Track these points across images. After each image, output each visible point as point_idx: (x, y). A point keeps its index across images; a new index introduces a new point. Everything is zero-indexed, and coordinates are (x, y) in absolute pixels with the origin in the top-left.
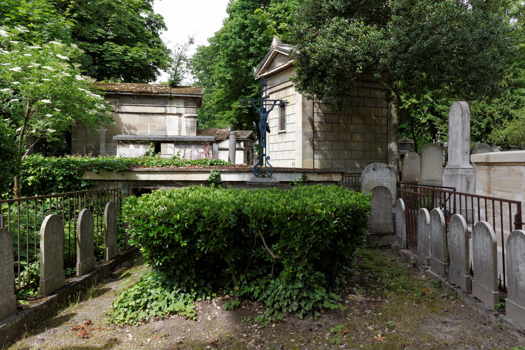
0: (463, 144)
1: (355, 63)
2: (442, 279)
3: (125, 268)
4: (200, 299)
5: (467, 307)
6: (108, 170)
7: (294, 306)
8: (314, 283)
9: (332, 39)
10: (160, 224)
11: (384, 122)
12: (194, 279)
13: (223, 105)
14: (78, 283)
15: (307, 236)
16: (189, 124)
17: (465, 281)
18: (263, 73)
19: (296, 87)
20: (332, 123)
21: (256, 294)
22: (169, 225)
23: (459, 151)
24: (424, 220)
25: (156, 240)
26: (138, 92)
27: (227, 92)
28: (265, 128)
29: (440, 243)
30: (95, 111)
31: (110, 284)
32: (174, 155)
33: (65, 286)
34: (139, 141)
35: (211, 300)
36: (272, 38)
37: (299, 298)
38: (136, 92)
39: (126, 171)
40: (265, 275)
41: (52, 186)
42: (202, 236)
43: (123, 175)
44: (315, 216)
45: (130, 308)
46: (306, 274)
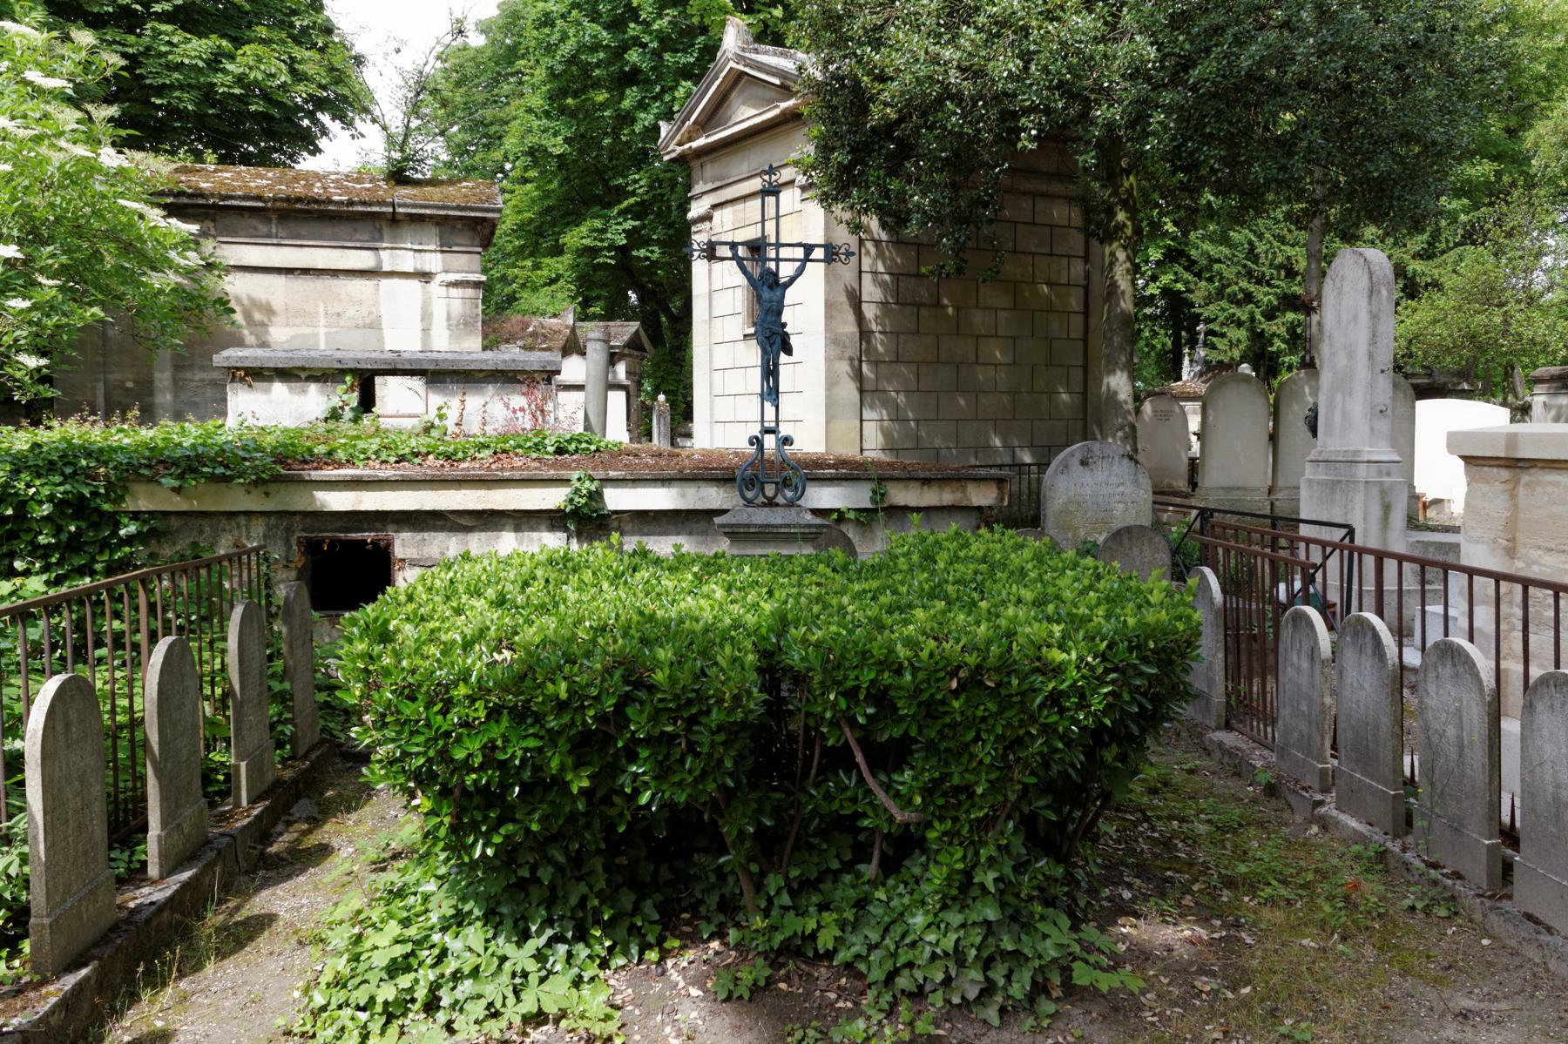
0: (1371, 385)
1: (1015, 116)
2: (1389, 844)
3: (305, 827)
4: (621, 961)
5: (1500, 945)
6: (213, 478)
7: (970, 982)
8: (1031, 898)
9: (940, 35)
10: (494, 714)
11: (1075, 303)
12: (599, 894)
13: (540, 237)
14: (160, 908)
15: (1018, 743)
16: (457, 307)
17: (1484, 858)
18: (690, 140)
19: (803, 189)
20: (919, 305)
21: (825, 940)
22: (521, 715)
23: (1358, 407)
24: (1306, 647)
25: (475, 771)
26: (282, 200)
27: (547, 195)
28: (779, 341)
29: (1377, 727)
30: (173, 278)
31: (265, 893)
32: (426, 418)
33: (115, 928)
34: (303, 369)
35: (661, 961)
36: (723, 24)
37: (985, 954)
38: (275, 200)
39: (278, 479)
40: (848, 867)
41: (12, 536)
42: (644, 753)
43: (267, 494)
44: (1043, 674)
46: (1008, 871)
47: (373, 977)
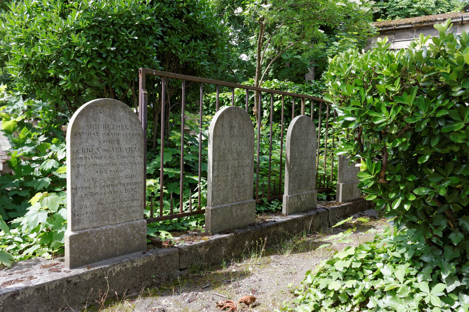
14: (277, 225)
26: (418, 23)
38: (416, 23)
45: (332, 295)
47: (335, 275)
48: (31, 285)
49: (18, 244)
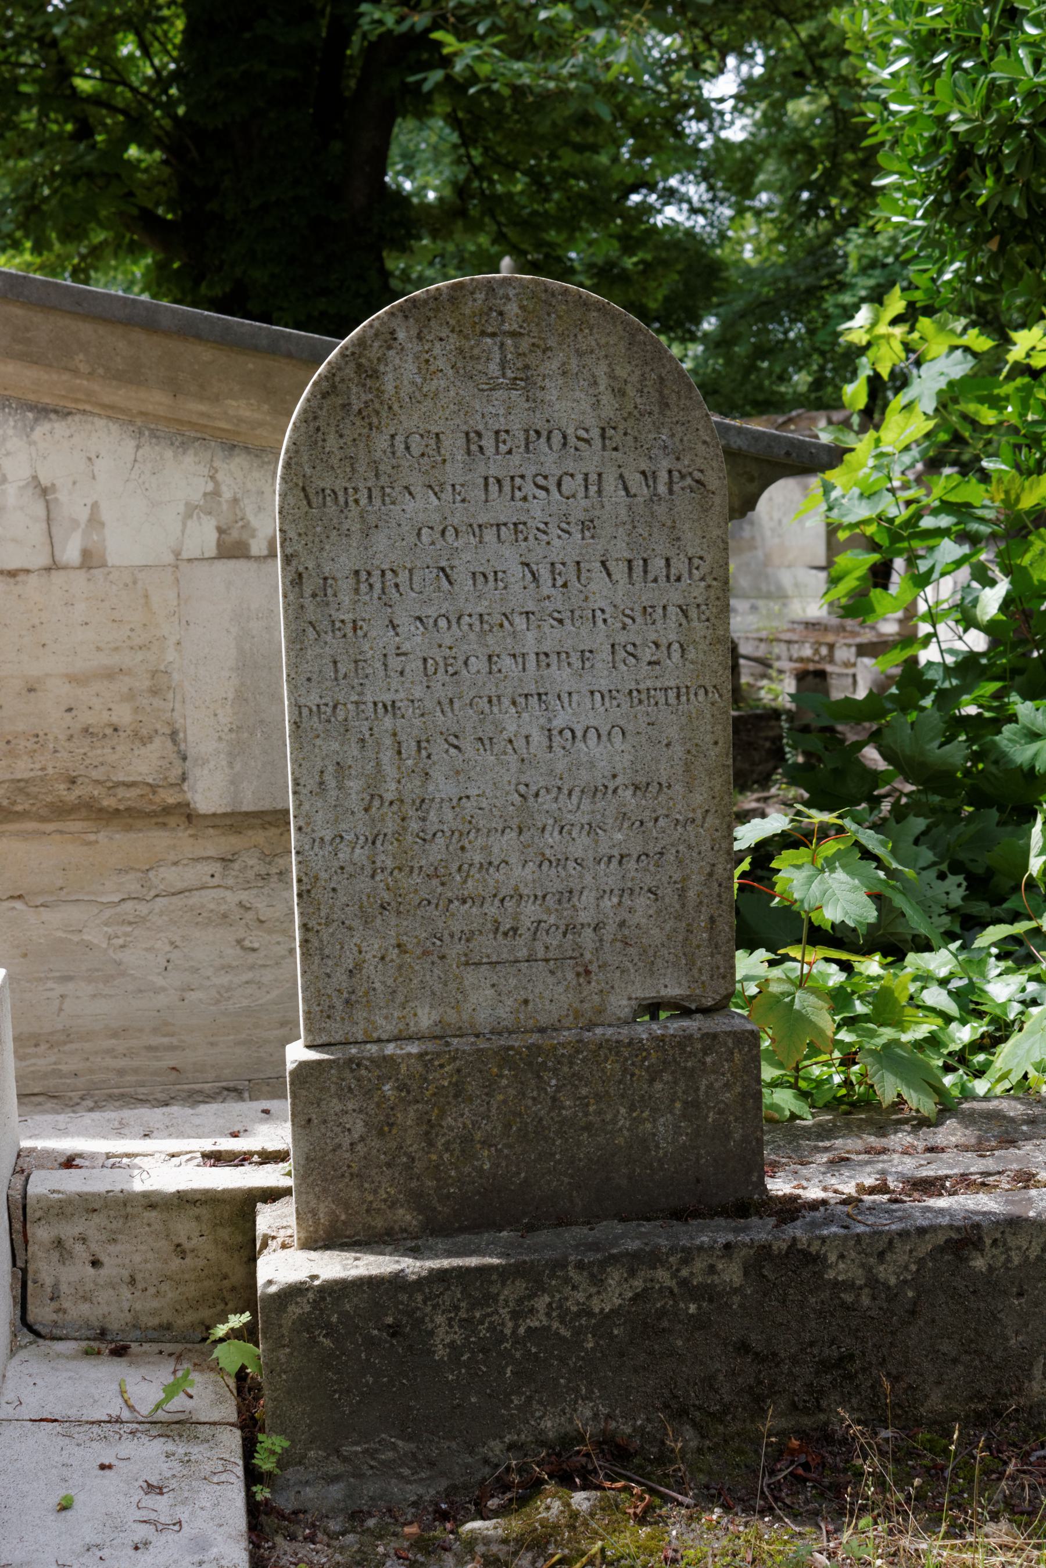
48: (1031, 1214)
49: (940, 1021)
